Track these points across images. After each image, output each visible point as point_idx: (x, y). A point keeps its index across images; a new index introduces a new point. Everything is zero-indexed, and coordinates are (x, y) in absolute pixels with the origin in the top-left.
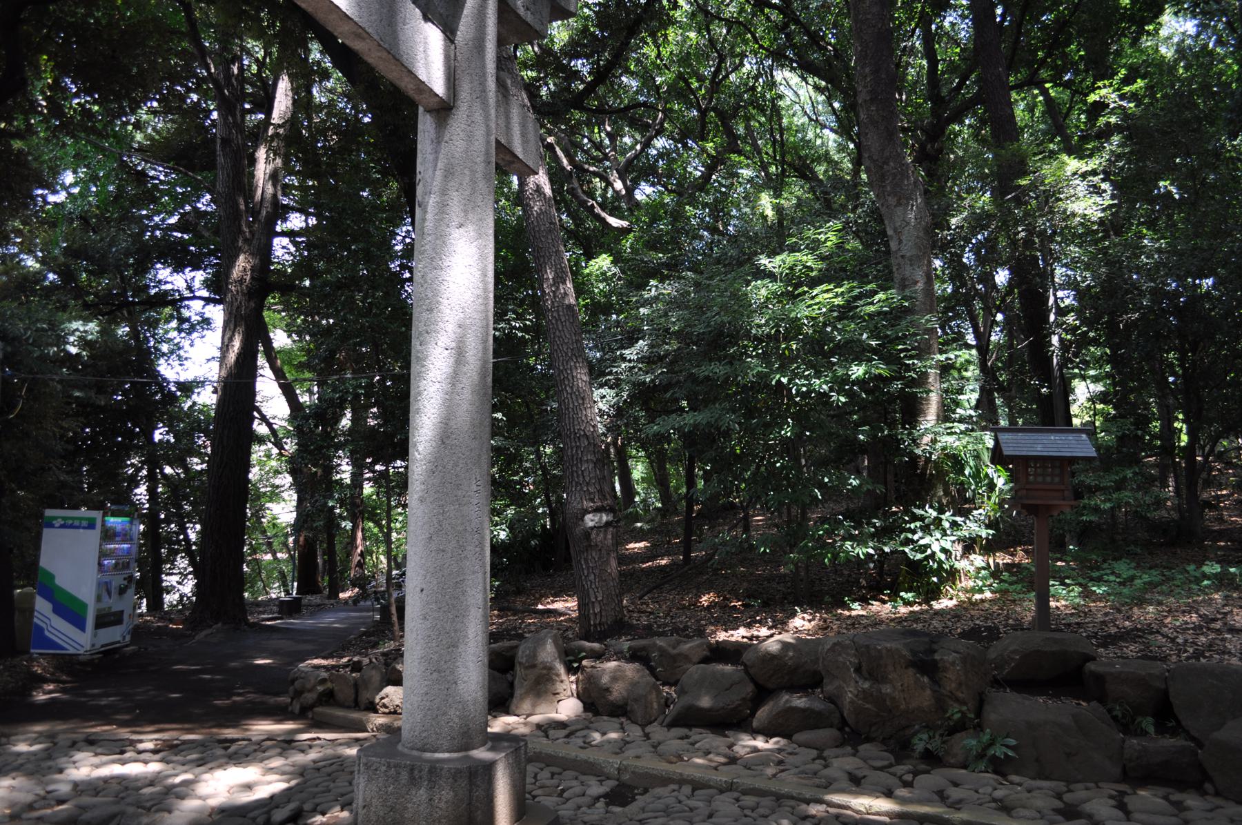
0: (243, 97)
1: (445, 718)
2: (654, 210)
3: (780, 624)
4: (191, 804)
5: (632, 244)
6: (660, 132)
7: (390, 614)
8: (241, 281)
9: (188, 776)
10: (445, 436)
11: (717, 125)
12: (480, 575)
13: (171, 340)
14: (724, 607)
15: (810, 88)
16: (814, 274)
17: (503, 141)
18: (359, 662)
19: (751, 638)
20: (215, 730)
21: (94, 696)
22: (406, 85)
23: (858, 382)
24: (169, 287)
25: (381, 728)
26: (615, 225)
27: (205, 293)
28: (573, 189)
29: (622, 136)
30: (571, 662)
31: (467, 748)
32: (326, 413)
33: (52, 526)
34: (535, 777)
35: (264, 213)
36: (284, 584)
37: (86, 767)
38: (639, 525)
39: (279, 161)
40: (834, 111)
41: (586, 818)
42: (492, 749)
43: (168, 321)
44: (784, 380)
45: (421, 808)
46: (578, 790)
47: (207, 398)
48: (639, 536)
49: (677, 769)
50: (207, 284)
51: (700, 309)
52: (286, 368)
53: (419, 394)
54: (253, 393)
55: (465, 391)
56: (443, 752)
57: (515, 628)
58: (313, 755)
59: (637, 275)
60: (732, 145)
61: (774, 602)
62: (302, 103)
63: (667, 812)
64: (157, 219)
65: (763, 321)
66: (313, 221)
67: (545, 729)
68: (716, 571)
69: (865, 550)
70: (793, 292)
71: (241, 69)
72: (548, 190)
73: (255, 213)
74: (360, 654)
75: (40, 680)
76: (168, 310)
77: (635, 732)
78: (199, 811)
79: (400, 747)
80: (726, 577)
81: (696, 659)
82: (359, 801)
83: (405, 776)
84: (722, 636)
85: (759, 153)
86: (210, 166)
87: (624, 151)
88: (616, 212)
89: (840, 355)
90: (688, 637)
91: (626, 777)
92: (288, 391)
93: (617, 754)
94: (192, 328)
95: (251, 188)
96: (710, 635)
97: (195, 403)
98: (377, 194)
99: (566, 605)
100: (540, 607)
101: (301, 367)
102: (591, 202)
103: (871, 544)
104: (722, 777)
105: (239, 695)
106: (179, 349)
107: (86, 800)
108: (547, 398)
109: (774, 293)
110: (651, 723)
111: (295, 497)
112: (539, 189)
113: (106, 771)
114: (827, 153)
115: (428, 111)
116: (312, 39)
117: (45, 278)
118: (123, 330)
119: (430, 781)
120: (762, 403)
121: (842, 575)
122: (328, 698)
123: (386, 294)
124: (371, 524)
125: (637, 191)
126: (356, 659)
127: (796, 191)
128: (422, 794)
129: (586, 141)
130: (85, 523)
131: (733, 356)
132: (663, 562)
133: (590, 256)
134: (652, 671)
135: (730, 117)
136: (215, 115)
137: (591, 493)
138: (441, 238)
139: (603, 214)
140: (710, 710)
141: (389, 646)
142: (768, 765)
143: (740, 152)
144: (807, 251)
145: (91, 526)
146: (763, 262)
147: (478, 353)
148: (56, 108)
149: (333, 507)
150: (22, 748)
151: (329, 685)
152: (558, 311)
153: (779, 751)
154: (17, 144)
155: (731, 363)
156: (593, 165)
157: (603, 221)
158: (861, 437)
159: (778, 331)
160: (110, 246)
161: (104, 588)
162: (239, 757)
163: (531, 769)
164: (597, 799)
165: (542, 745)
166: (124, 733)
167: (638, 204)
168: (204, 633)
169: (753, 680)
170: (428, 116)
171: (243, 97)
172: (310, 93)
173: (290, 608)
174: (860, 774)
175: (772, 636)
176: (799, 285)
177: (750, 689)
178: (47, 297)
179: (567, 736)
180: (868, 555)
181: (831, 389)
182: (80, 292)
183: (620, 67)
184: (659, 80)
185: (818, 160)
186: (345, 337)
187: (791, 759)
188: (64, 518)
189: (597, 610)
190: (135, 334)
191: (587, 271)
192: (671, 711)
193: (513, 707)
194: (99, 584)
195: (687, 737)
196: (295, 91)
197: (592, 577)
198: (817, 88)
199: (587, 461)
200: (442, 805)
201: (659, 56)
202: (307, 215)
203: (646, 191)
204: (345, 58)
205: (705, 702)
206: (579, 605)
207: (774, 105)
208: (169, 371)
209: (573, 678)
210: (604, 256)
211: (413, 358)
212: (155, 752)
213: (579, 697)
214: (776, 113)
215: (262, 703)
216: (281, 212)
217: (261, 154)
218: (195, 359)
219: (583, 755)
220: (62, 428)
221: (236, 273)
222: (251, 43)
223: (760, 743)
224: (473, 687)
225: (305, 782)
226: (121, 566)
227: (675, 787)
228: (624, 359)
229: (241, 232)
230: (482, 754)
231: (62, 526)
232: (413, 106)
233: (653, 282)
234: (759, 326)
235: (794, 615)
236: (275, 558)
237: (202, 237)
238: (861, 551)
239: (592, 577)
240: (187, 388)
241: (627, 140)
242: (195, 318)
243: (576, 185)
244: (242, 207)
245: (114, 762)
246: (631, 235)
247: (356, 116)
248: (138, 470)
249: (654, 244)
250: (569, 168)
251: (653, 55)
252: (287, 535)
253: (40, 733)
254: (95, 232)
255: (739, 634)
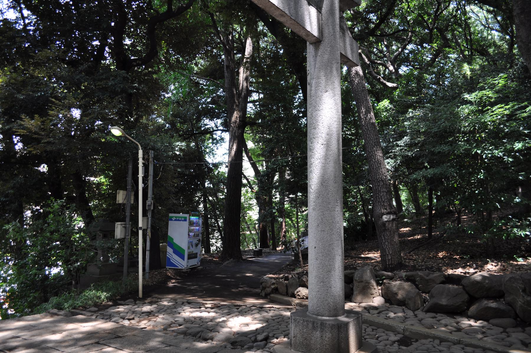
0: (233, 48)
1: (326, 302)
2: (408, 77)
3: (480, 267)
4: (226, 330)
5: (398, 94)
6: (410, 42)
7: (299, 257)
8: (235, 122)
9: (224, 319)
10: (323, 182)
11: (437, 35)
12: (340, 242)
13: (210, 147)
14: (450, 258)
15: (485, 12)
16: (493, 100)
17: (343, 53)
18: (288, 277)
19: (465, 273)
20: (233, 301)
21: (188, 285)
22: (302, 34)
23: (519, 151)
24: (208, 126)
25: (298, 304)
26: (390, 86)
27: (221, 128)
28: (370, 72)
29: (392, 46)
30: (378, 280)
31: (336, 315)
32: (269, 174)
33: (172, 220)
34: (365, 330)
35: (243, 94)
36: (255, 244)
37: (188, 313)
38: (406, 220)
39: (248, 72)
40: (498, 21)
41: (390, 350)
42: (347, 317)
43: (208, 140)
44: (479, 152)
45: (318, 340)
46: (385, 337)
47: (224, 170)
48: (406, 225)
49: (432, 332)
50: (222, 124)
51: (435, 121)
52: (252, 156)
53: (312, 164)
54: (241, 166)
55: (331, 162)
56: (326, 316)
57: (352, 265)
58: (271, 314)
59: (402, 108)
60: (446, 43)
61: (479, 258)
62: (256, 48)
63: (417, 349)
64: (203, 100)
65: (467, 124)
66: (262, 96)
67: (368, 309)
68: (445, 242)
69: (524, 233)
70: (482, 110)
71: (233, 37)
72: (361, 73)
73: (239, 95)
74: (288, 273)
75: (170, 278)
76: (208, 136)
77: (410, 313)
78: (230, 333)
79: (308, 313)
80: (449, 244)
81: (438, 282)
82: (292, 334)
83: (310, 325)
84: (450, 272)
85: (459, 46)
86: (222, 77)
87: (393, 52)
88: (390, 80)
89: (508, 139)
90: (433, 271)
91: (407, 333)
92: (254, 166)
93: (402, 323)
94: (217, 142)
95: (238, 84)
96: (444, 271)
97: (219, 172)
98: (287, 81)
99: (375, 255)
100: (363, 256)
101: (259, 155)
102: (379, 77)
103: (527, 230)
104: (455, 337)
105: (241, 288)
106: (213, 150)
107: (188, 325)
108: (362, 164)
109: (472, 111)
110: (418, 309)
111: (258, 208)
112: (357, 73)
113: (197, 314)
114: (494, 42)
115: (311, 44)
116: (259, 21)
117: (166, 126)
118: (193, 144)
119: (321, 328)
120: (469, 162)
121: (511, 244)
122: (276, 291)
123: (293, 123)
124: (288, 220)
125: (399, 70)
126: (286, 275)
127: (479, 62)
128: (318, 334)
129: (375, 50)
130: (183, 219)
131: (452, 142)
132: (419, 237)
133: (379, 100)
134: (417, 286)
135: (444, 30)
136: (223, 57)
137: (385, 206)
138: (318, 98)
139: (385, 82)
140: (446, 306)
141: (300, 270)
142: (478, 334)
143: (450, 47)
144: (489, 90)
145: (185, 220)
146: (466, 96)
147: (336, 146)
148: (167, 60)
149: (275, 213)
150: (165, 303)
151: (276, 285)
152: (367, 126)
153: (483, 327)
154: (155, 76)
155: (451, 145)
156: (379, 60)
157: (385, 85)
158: (521, 178)
159: (475, 129)
160: (187, 112)
161: (190, 244)
162: (243, 312)
163: (364, 326)
164: (394, 342)
165: (367, 315)
166: (200, 300)
167: (401, 76)
168: (226, 262)
169: (467, 293)
170: (311, 46)
171: (233, 48)
172: (259, 43)
173: (258, 253)
174: (527, 341)
175: (476, 272)
176: (485, 106)
177: (466, 297)
178: (167, 134)
179: (378, 313)
180: (526, 235)
181: (504, 155)
182: (177, 131)
183: (391, 14)
184: (409, 18)
185: (490, 46)
186: (278, 142)
187: (489, 332)
188: (176, 217)
189: (390, 258)
190: (197, 145)
191: (378, 108)
192: (427, 305)
193: (353, 299)
194: (189, 242)
195: (435, 317)
196: (254, 43)
197: (387, 243)
198: (488, 11)
199: (383, 192)
200: (326, 339)
201: (409, 7)
202: (259, 93)
203: (403, 70)
204: (275, 26)
205: (444, 302)
206: (381, 256)
207: (466, 23)
208: (210, 159)
209: (380, 288)
210: (386, 100)
211: (308, 149)
212: (212, 308)
213: (382, 296)
214: (467, 26)
215: (250, 291)
216: (249, 93)
217: (241, 70)
218: (219, 154)
219: (386, 322)
220: (173, 182)
221: (233, 119)
222: (236, 26)
223: (472, 322)
224: (338, 290)
225: (269, 325)
226: (196, 236)
227: (432, 340)
228: (398, 146)
229: (235, 102)
230: (343, 318)
231: (175, 220)
232: (304, 42)
233: (410, 110)
234: (465, 127)
235: (487, 263)
236: (251, 233)
237: (220, 106)
238: (522, 233)
239: (387, 243)
240: (216, 166)
241: (394, 47)
242: (218, 138)
243: (372, 70)
244: (235, 92)
245: (197, 311)
246: (398, 90)
247: (277, 50)
248: (200, 198)
249: (409, 93)
250: (368, 63)
251: (406, 7)
252: (255, 224)
253: (171, 299)
254: (182, 107)
255: (459, 271)
